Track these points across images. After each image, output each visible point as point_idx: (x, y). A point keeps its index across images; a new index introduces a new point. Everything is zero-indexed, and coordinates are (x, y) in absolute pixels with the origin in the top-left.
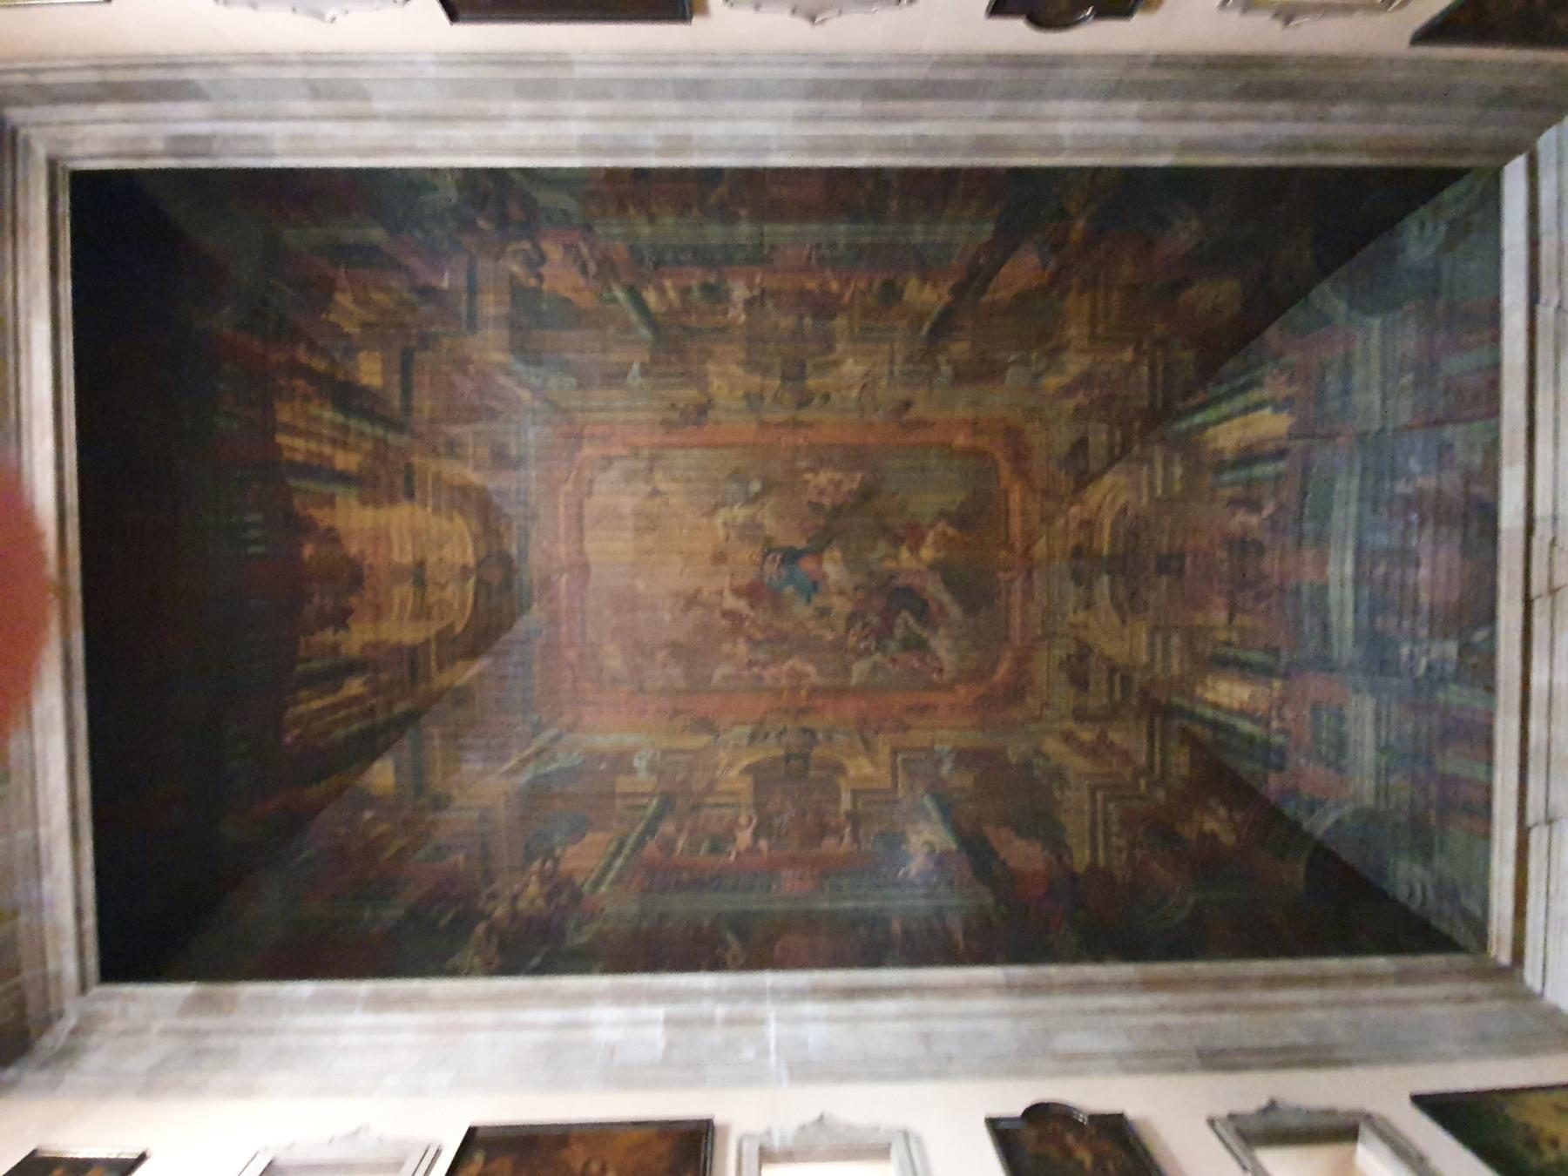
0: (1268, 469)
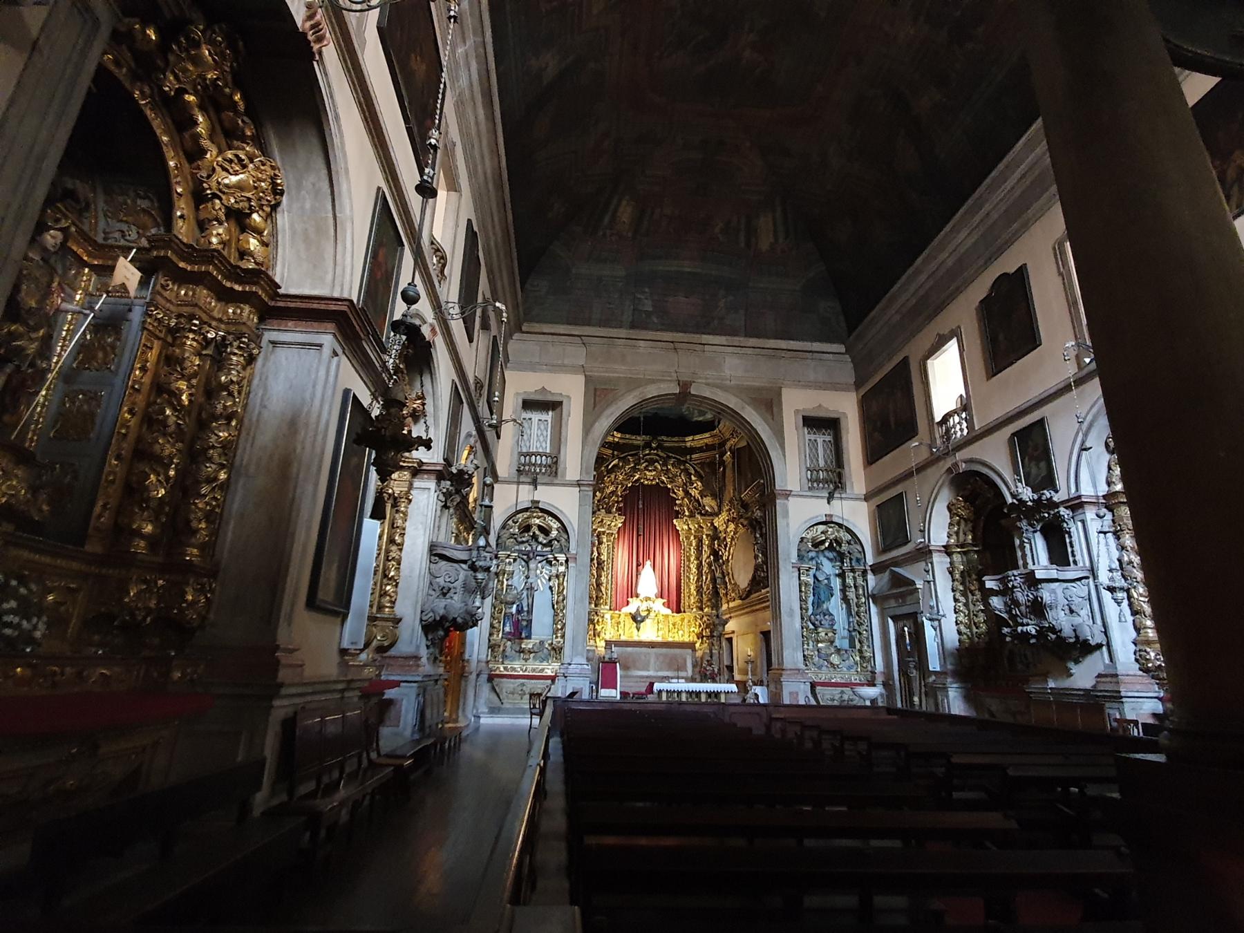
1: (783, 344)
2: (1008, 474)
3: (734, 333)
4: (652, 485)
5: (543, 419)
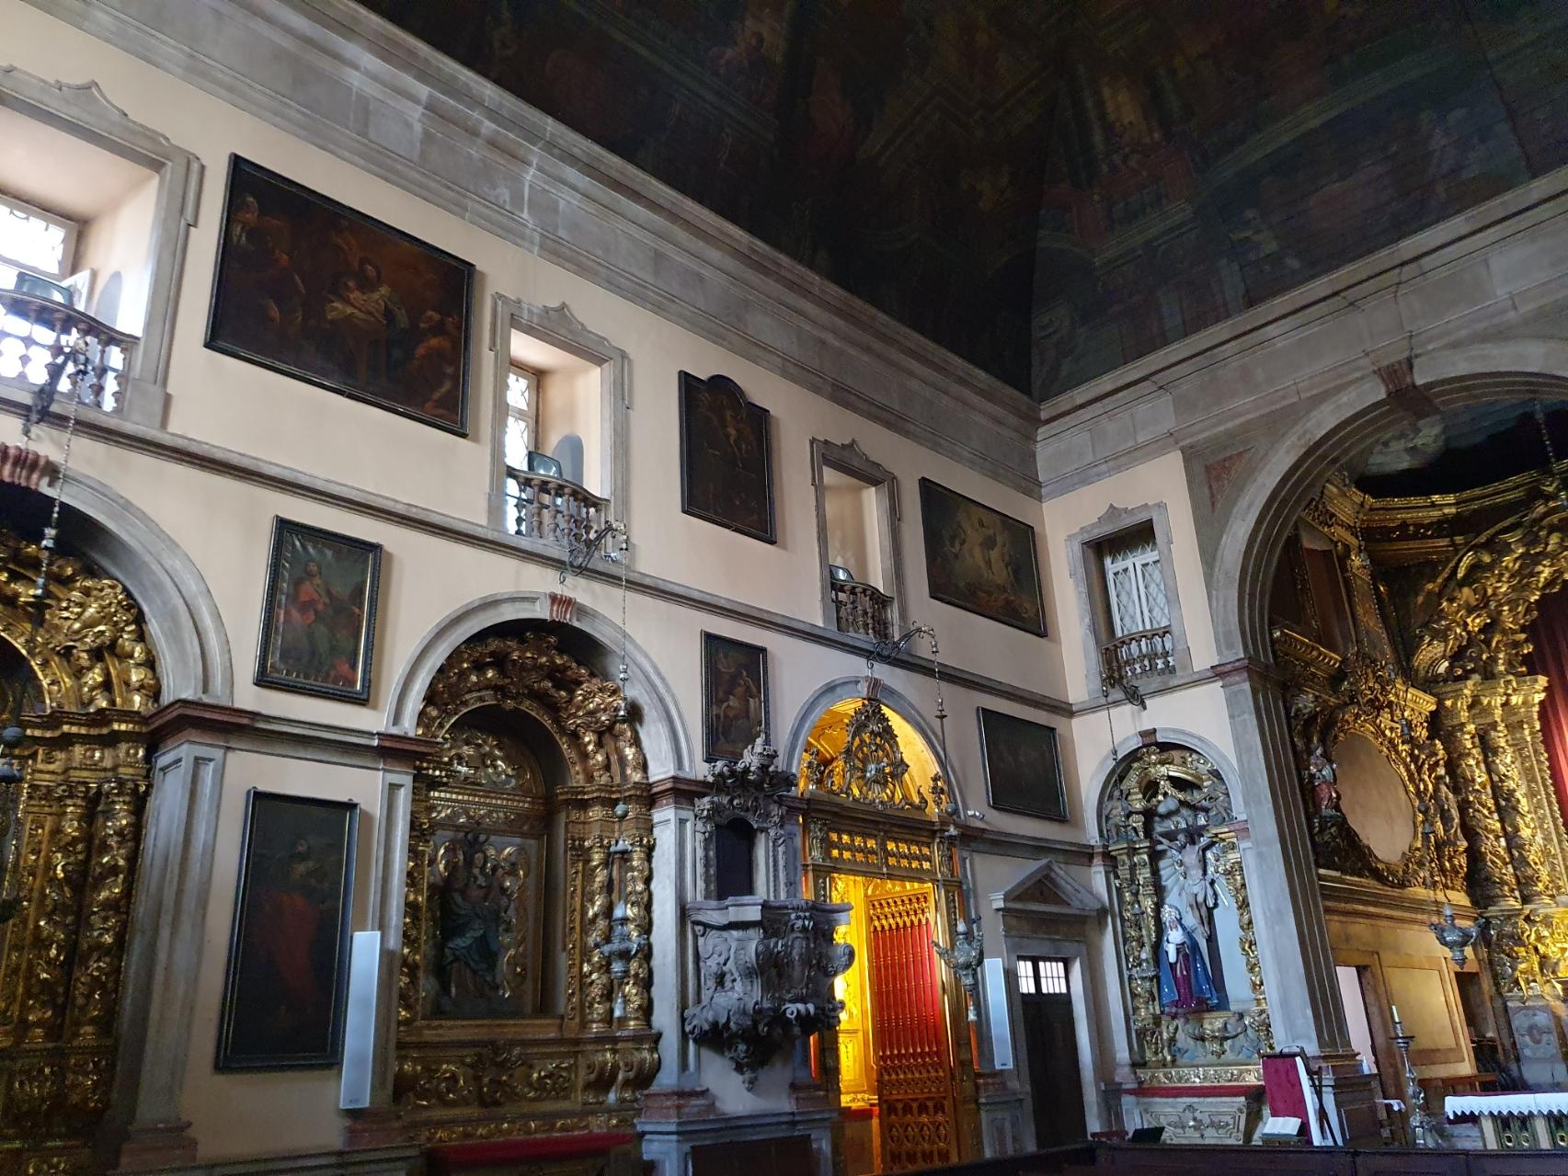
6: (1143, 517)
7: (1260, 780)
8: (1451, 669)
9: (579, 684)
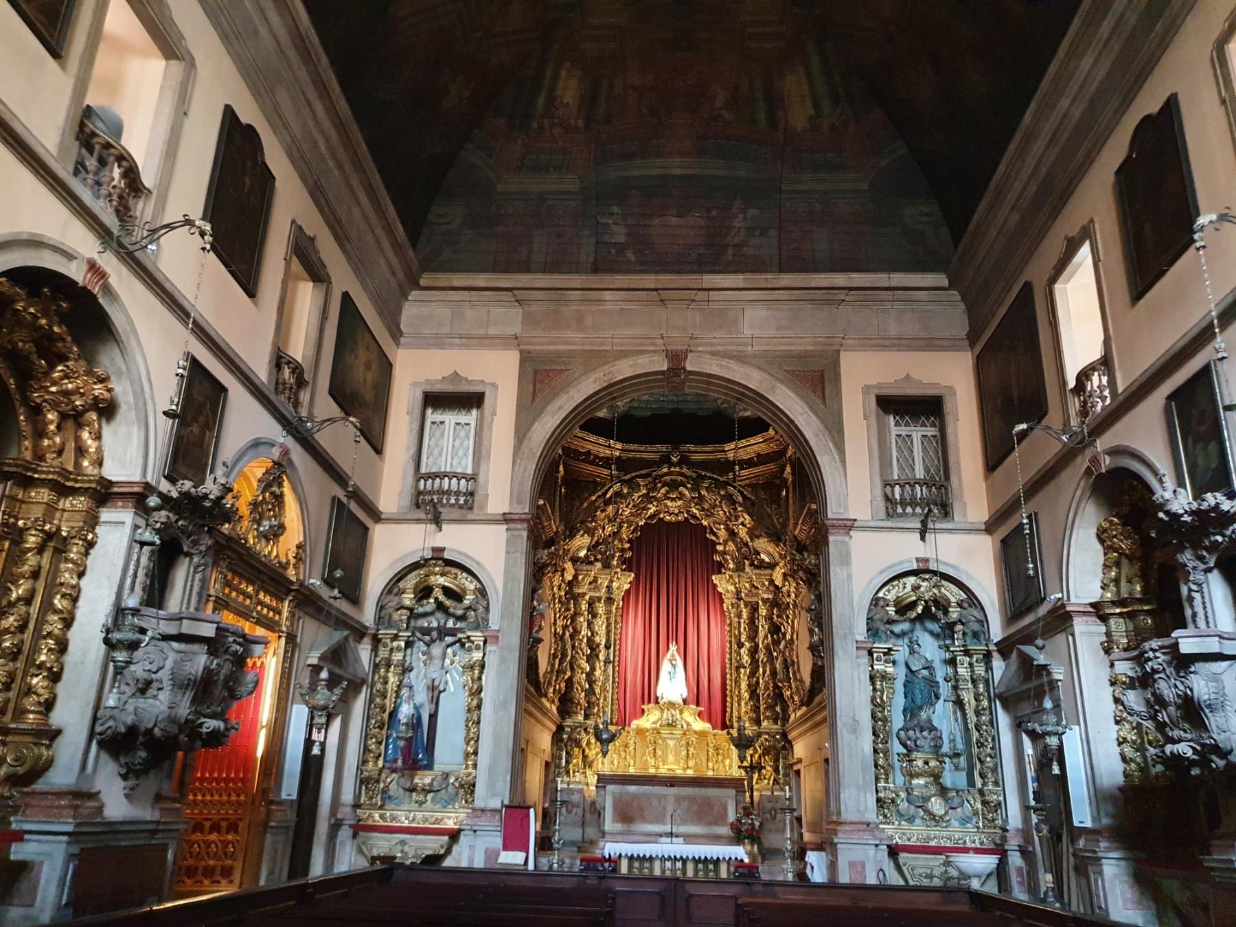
0: (762, 116)
1: (840, 279)
2: (1164, 465)
3: (758, 266)
4: (678, 523)
5: (463, 422)
6: (479, 389)
7: (516, 603)
8: (586, 556)
9: (63, 358)
